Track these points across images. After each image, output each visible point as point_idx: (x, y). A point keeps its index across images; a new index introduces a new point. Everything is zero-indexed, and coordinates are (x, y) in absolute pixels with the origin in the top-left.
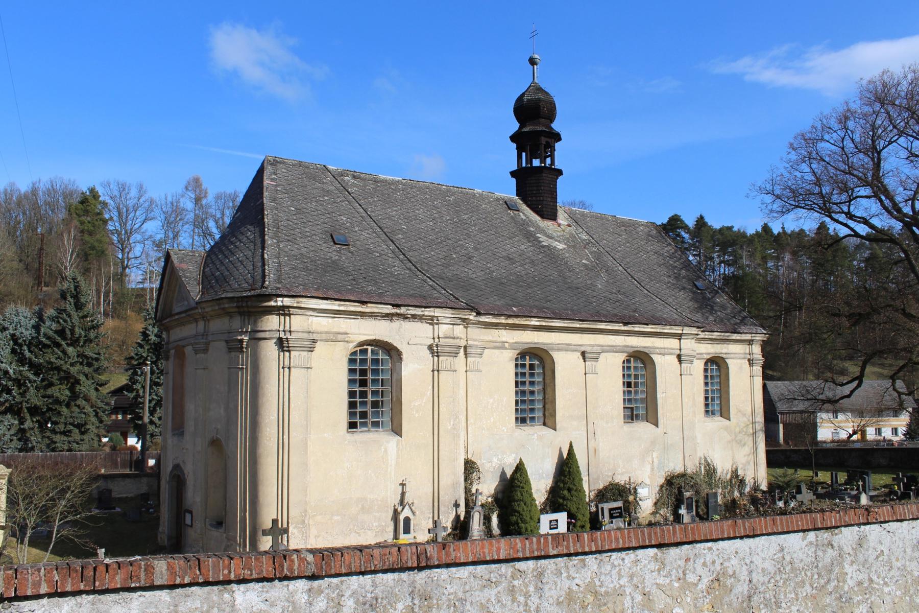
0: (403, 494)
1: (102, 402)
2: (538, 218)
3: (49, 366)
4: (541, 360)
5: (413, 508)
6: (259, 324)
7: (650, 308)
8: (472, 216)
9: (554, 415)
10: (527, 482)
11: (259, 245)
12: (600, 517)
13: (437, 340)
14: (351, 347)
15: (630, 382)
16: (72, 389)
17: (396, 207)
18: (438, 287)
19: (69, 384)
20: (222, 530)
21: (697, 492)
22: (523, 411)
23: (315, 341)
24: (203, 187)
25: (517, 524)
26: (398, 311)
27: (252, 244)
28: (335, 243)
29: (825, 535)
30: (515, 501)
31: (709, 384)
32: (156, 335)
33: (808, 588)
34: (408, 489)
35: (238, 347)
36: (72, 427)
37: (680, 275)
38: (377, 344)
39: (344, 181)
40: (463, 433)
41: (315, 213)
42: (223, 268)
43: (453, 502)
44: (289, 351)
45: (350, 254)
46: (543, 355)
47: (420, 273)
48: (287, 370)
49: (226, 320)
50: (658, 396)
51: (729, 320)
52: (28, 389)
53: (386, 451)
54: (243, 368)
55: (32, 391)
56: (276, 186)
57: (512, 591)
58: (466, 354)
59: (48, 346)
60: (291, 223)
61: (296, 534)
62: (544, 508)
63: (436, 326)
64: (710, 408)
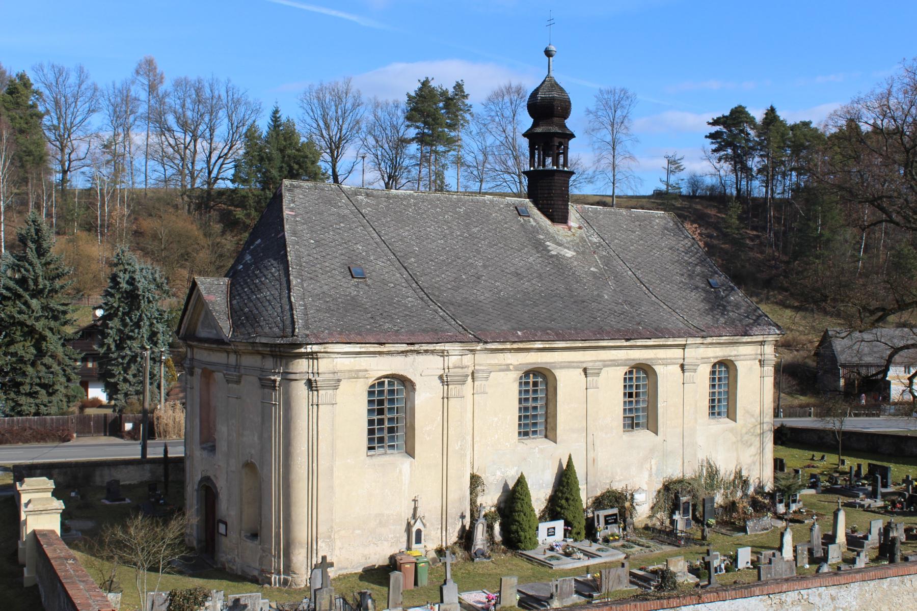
0: (415, 509)
2: (549, 222)
3: (12, 321)
4: (544, 377)
5: (424, 521)
6: (291, 367)
7: (655, 318)
8: (482, 228)
9: (554, 429)
10: (527, 494)
11: (285, 285)
12: (596, 524)
13: (447, 370)
15: (632, 393)
17: (408, 226)
18: (448, 318)
19: (34, 340)
20: (257, 542)
21: (694, 497)
22: (526, 425)
23: (339, 380)
24: (158, 71)
26: (412, 348)
27: (277, 282)
30: (515, 511)
31: (717, 386)
32: (128, 283)
34: (419, 504)
35: (272, 385)
36: (38, 388)
37: (694, 272)
42: (251, 304)
44: (317, 390)
45: (367, 288)
46: (546, 373)
47: (431, 303)
48: (315, 407)
50: (659, 405)
51: (740, 321)
53: (400, 471)
54: (276, 404)
56: (295, 216)
58: (473, 378)
59: (9, 299)
60: (312, 259)
61: (324, 547)
62: (544, 515)
63: (446, 358)
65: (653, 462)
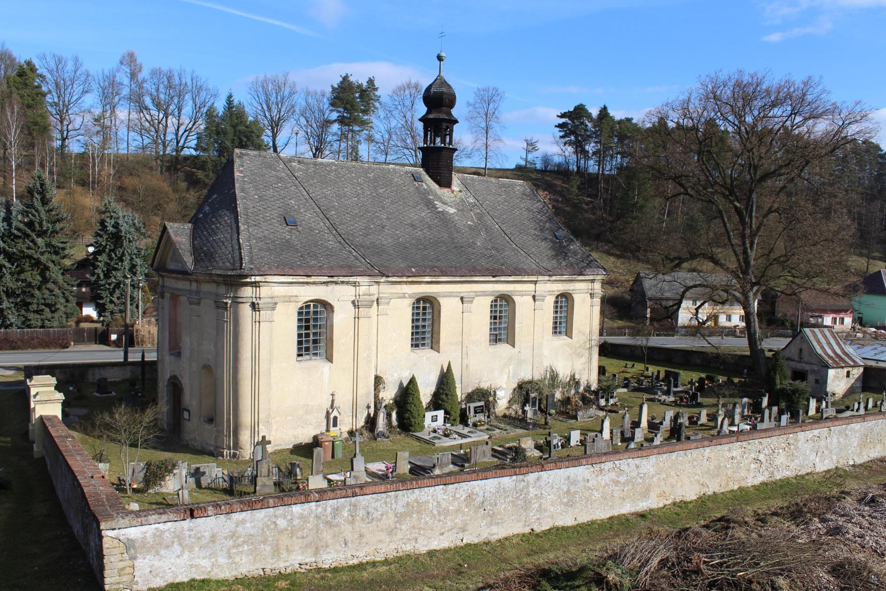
0: (333, 401)
1: (68, 284)
2: (437, 186)
4: (431, 303)
9: (438, 342)
10: (417, 391)
11: (235, 230)
12: (468, 413)
13: (358, 297)
14: (300, 305)
16: (43, 274)
21: (540, 393)
22: (417, 339)
23: (276, 304)
24: (138, 62)
25: (409, 418)
28: (287, 225)
29: (521, 477)
30: (408, 403)
32: (113, 226)
33: (510, 498)
34: (336, 398)
35: (225, 306)
36: (43, 307)
38: (318, 302)
39: (291, 166)
40: (374, 359)
41: (272, 200)
42: (209, 245)
43: (366, 405)
44: (259, 311)
46: (433, 300)
48: (257, 323)
49: (214, 285)
51: (577, 264)
52: (5, 274)
53: (322, 373)
55: (8, 276)
56: (244, 177)
57: (386, 503)
59: (19, 237)
64: (558, 330)
65: (511, 368)
